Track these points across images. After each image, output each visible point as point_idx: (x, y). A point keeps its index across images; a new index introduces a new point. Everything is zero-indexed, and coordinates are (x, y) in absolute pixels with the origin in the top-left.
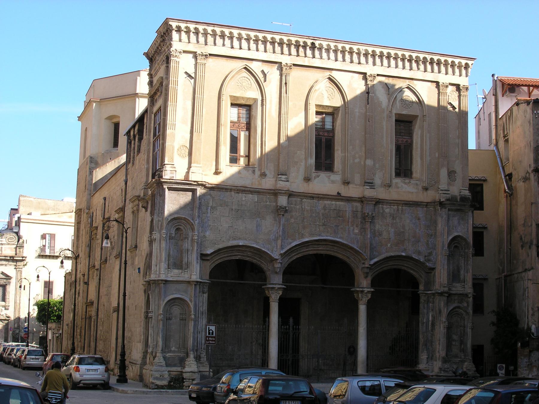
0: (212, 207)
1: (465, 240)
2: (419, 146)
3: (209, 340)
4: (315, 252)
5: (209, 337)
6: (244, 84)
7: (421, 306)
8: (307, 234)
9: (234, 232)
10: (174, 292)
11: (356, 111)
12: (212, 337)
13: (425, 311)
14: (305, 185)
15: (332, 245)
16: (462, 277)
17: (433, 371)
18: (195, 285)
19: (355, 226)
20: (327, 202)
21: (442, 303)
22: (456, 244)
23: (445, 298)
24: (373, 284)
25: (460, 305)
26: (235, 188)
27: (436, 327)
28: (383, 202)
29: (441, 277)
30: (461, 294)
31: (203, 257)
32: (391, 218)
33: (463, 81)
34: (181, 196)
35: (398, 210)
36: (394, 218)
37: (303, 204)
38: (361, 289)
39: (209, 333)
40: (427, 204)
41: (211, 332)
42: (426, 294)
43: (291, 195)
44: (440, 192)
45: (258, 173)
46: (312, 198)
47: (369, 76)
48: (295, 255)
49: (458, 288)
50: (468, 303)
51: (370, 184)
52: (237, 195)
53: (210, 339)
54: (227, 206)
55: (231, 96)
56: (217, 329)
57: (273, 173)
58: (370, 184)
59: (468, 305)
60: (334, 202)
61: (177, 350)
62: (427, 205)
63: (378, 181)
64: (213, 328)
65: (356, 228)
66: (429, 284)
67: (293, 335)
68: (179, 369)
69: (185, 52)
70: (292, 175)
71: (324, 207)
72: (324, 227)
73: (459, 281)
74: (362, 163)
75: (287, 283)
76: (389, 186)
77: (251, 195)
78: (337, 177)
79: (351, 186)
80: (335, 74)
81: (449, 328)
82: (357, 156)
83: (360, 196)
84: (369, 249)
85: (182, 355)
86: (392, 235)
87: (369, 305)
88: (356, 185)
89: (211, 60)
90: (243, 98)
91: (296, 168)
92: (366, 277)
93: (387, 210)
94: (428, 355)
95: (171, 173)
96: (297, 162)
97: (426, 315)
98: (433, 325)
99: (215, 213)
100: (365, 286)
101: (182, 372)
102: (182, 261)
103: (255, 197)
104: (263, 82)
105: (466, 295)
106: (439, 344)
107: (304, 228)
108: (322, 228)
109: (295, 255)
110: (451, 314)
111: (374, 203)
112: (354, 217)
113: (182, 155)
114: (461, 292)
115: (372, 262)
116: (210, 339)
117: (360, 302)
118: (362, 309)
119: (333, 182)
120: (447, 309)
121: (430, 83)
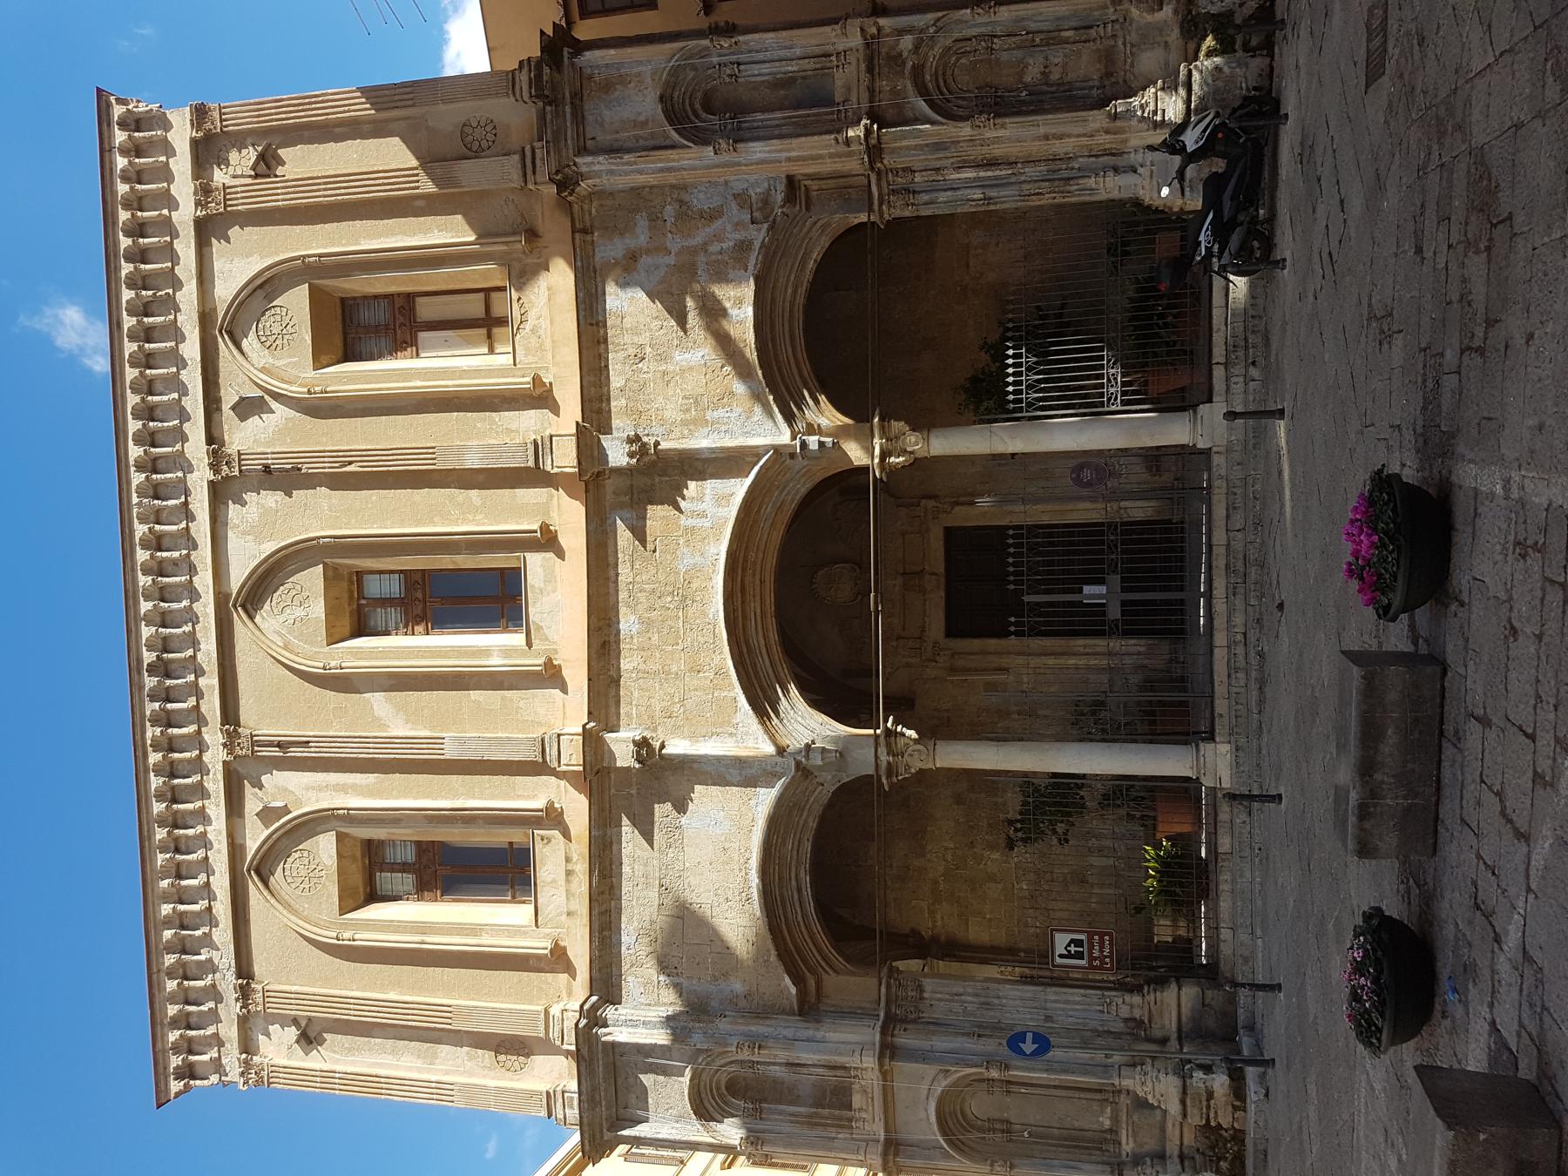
1: (675, 72)
3: (1102, 959)
5: (1092, 958)
6: (303, 873)
7: (926, 212)
13: (943, 197)
15: (744, 570)
16: (809, 64)
29: (814, 154)
30: (870, 70)
31: (809, 1008)
33: (181, 134)
39: (1079, 956)
49: (847, 79)
50: (901, 32)
53: (1096, 953)
66: (844, 190)
94: (1105, 169)
98: (992, 163)
105: (871, 46)
106: (1061, 137)
114: (863, 66)
116: (1096, 953)
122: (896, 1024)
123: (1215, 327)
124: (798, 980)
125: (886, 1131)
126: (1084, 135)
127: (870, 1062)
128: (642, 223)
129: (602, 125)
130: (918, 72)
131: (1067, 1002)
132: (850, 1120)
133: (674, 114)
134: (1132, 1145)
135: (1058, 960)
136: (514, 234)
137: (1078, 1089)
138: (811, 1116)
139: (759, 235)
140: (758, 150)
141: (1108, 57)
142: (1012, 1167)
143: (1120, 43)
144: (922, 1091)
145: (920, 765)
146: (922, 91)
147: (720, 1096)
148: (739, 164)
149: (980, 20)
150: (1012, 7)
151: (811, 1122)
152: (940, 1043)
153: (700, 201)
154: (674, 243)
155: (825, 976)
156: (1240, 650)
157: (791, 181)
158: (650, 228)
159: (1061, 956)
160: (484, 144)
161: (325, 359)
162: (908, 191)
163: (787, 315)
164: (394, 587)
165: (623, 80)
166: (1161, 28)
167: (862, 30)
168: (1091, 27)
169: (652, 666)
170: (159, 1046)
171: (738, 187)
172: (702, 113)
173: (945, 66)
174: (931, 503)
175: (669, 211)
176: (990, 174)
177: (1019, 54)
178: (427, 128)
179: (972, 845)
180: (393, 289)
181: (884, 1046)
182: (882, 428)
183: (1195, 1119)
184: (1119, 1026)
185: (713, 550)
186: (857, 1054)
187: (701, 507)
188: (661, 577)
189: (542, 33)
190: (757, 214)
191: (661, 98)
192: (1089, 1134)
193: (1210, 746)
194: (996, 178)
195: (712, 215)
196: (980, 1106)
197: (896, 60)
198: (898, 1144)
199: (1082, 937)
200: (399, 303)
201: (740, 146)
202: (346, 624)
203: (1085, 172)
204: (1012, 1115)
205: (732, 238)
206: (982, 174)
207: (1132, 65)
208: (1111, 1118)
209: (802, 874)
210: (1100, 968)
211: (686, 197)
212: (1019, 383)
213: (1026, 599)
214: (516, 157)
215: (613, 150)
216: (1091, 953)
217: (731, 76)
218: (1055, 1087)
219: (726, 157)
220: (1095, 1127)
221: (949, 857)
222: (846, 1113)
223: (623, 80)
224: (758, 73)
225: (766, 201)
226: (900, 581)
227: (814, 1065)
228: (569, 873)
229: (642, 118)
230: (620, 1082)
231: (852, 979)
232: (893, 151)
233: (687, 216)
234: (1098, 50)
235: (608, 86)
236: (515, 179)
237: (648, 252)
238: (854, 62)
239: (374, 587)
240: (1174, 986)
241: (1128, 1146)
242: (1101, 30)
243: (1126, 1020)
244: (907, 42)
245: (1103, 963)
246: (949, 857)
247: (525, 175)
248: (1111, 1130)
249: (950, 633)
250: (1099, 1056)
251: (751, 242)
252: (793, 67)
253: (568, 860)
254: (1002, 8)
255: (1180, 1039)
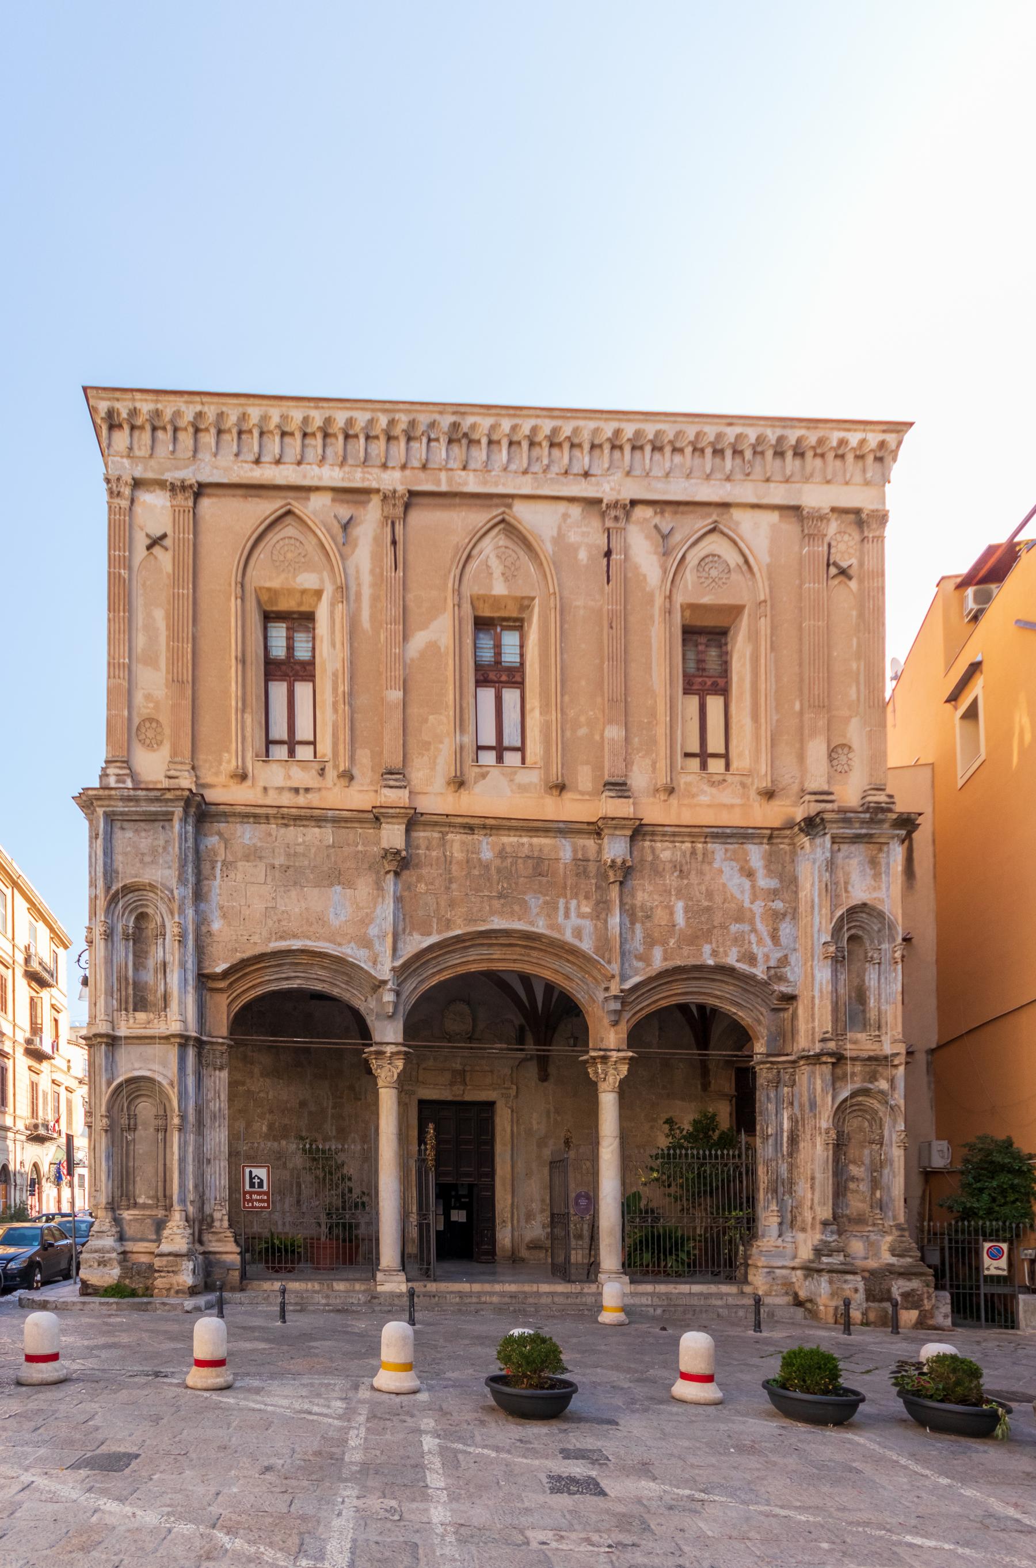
0: (224, 862)
1: (881, 915)
2: (747, 685)
3: (251, 1201)
4: (483, 967)
5: (251, 1193)
8: (459, 921)
9: (279, 921)
11: (578, 603)
12: (259, 1193)
13: (771, 1107)
15: (525, 947)
16: (872, 1015)
17: (795, 1257)
18: (181, 1045)
19: (581, 897)
20: (509, 840)
21: (819, 1082)
22: (853, 931)
23: (827, 1070)
25: (871, 1086)
27: (802, 1145)
28: (653, 834)
30: (870, 1059)
31: (204, 980)
32: (676, 874)
34: (143, 834)
35: (693, 853)
37: (448, 847)
38: (602, 1053)
40: (771, 835)
41: (256, 1181)
42: (772, 1063)
44: (807, 797)
46: (470, 829)
48: (434, 974)
50: (892, 1081)
51: (619, 788)
52: (283, 830)
53: (254, 1197)
54: (260, 858)
57: (370, 774)
58: (619, 788)
59: (893, 1087)
60: (525, 840)
61: (150, 1202)
62: (770, 837)
63: (639, 779)
65: (584, 902)
66: (784, 1035)
70: (418, 775)
71: (500, 852)
72: (502, 901)
73: (865, 1026)
74: (597, 737)
75: (413, 1039)
76: (671, 791)
77: (317, 830)
79: (568, 796)
81: (839, 1146)
82: (583, 719)
84: (618, 950)
86: (680, 919)
87: (624, 1090)
88: (582, 793)
91: (426, 758)
92: (615, 1023)
93: (665, 855)
94: (782, 1216)
96: (429, 743)
97: (775, 1118)
98: (794, 1140)
99: (232, 876)
103: (327, 834)
105: (884, 1060)
107: (452, 904)
109: (434, 974)
110: (841, 1111)
111: (629, 833)
112: (577, 875)
114: (872, 1054)
115: (627, 986)
116: (254, 1197)
117: (603, 1086)
118: (608, 1102)
119: (523, 788)
120: (834, 1099)
122: (194, 1045)
123: (678, 1286)
124: (225, 974)
125: (126, 1038)
126: (812, 1204)
127: (175, 1027)
128: (774, 883)
129: (847, 857)
130: (866, 1092)
131: (220, 1175)
132: (126, 1010)
133: (853, 911)
134: (128, 1218)
135: (247, 1170)
136: (772, 782)
137: (165, 1181)
138: (127, 979)
139: (759, 972)
140: (823, 974)
141: (860, 1220)
142: (106, 1131)
143: (870, 1228)
144: (161, 1066)
145: (383, 1075)
146: (854, 1095)
147: (137, 906)
148: (813, 960)
149: (894, 1136)
150: (902, 1159)
151: (123, 979)
152: (191, 1081)
153: (786, 929)
154: (758, 908)
155: (226, 995)
156: (474, 1300)
157: (791, 998)
158: (769, 889)
159: (251, 1172)
160: (835, 763)
161: (687, 613)
162: (778, 1082)
163: (703, 990)
164: (773, 655)
165: (877, 876)
166: (877, 1255)
167: (898, 1054)
168: (881, 1210)
170: (138, 396)
171: (792, 959)
172: (854, 932)
173: (865, 1111)
174: (513, 1092)
175: (779, 905)
176: (785, 1139)
177: (867, 1161)
178: (851, 717)
179: (271, 1112)
180: (735, 678)
181: (187, 1038)
182: (624, 1058)
183: (158, 1263)
184: (207, 1210)
185: (541, 923)
186: (106, 1018)
187: (573, 914)
189: (920, 814)
190: (772, 972)
191: (865, 905)
192: (131, 1187)
193: (404, 1278)
194: (782, 1144)
195: (775, 938)
196: (145, 1109)
197: (873, 1077)
198: (113, 1045)
200: (721, 682)
201: (829, 961)
203: (781, 1203)
204: (141, 1132)
205: (759, 951)
206: (785, 1134)
207: (856, 1236)
208: (144, 1204)
209: (299, 982)
210: (245, 1200)
211: (788, 919)
214: (825, 788)
215: (831, 865)
217: (872, 957)
218: (165, 1165)
219: (819, 950)
220: (137, 1192)
221: (262, 1095)
222: (131, 1007)
223: (877, 876)
224: (871, 978)
225: (781, 978)
226: (459, 1067)
227: (165, 983)
228: (296, 790)
229: (850, 888)
230: (142, 824)
231: (225, 1016)
232: (813, 1073)
233: (777, 917)
234: (864, 1214)
235: (874, 862)
236: (812, 785)
237: (753, 887)
238: (873, 1047)
239: (510, 640)
240: (238, 1250)
241: (127, 1215)
242: (879, 1216)
243: (211, 1216)
244: (883, 1085)
245: (249, 1201)
246: (262, 1095)
247: (815, 793)
248: (136, 1203)
249: (422, 1103)
250: (191, 1196)
251: (755, 966)
252: (872, 1003)
253: (307, 790)
254: (902, 1152)
255: (204, 1253)
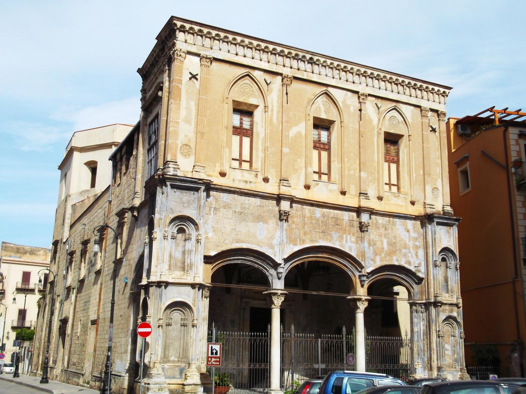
0: (215, 208)
5: (211, 358)
8: (308, 241)
9: (237, 235)
10: (176, 295)
12: (215, 358)
14: (341, 196)
19: (351, 234)
24: (369, 293)
26: (238, 190)
35: (389, 221)
36: (386, 229)
39: (212, 353)
41: (214, 351)
43: (292, 200)
45: (261, 177)
47: (361, 95)
54: (230, 208)
55: (234, 101)
56: (222, 349)
63: (372, 193)
64: (217, 347)
65: (352, 237)
67: (295, 343)
68: (180, 381)
69: (189, 53)
71: (323, 215)
78: (335, 188)
80: (330, 89)
82: (352, 167)
83: (357, 206)
85: (183, 365)
88: (352, 195)
89: (214, 64)
90: (246, 104)
95: (174, 171)
96: (298, 170)
99: (218, 214)
100: (362, 295)
101: (183, 385)
102: (184, 263)
104: (266, 91)
107: (305, 234)
108: (321, 235)
112: (350, 226)
113: (184, 154)
119: (331, 191)
121: (413, 108)
154: (411, 244)
159: (212, 347)
169: (306, 219)
188: (330, 226)
199: (218, 355)
202: (317, 123)
212: (262, 337)
213: (319, 340)
216: (213, 357)
228: (246, 182)
237: (409, 236)
